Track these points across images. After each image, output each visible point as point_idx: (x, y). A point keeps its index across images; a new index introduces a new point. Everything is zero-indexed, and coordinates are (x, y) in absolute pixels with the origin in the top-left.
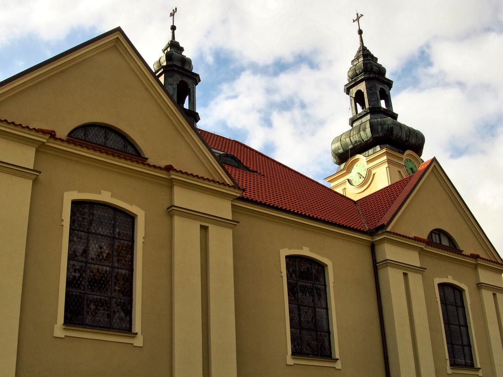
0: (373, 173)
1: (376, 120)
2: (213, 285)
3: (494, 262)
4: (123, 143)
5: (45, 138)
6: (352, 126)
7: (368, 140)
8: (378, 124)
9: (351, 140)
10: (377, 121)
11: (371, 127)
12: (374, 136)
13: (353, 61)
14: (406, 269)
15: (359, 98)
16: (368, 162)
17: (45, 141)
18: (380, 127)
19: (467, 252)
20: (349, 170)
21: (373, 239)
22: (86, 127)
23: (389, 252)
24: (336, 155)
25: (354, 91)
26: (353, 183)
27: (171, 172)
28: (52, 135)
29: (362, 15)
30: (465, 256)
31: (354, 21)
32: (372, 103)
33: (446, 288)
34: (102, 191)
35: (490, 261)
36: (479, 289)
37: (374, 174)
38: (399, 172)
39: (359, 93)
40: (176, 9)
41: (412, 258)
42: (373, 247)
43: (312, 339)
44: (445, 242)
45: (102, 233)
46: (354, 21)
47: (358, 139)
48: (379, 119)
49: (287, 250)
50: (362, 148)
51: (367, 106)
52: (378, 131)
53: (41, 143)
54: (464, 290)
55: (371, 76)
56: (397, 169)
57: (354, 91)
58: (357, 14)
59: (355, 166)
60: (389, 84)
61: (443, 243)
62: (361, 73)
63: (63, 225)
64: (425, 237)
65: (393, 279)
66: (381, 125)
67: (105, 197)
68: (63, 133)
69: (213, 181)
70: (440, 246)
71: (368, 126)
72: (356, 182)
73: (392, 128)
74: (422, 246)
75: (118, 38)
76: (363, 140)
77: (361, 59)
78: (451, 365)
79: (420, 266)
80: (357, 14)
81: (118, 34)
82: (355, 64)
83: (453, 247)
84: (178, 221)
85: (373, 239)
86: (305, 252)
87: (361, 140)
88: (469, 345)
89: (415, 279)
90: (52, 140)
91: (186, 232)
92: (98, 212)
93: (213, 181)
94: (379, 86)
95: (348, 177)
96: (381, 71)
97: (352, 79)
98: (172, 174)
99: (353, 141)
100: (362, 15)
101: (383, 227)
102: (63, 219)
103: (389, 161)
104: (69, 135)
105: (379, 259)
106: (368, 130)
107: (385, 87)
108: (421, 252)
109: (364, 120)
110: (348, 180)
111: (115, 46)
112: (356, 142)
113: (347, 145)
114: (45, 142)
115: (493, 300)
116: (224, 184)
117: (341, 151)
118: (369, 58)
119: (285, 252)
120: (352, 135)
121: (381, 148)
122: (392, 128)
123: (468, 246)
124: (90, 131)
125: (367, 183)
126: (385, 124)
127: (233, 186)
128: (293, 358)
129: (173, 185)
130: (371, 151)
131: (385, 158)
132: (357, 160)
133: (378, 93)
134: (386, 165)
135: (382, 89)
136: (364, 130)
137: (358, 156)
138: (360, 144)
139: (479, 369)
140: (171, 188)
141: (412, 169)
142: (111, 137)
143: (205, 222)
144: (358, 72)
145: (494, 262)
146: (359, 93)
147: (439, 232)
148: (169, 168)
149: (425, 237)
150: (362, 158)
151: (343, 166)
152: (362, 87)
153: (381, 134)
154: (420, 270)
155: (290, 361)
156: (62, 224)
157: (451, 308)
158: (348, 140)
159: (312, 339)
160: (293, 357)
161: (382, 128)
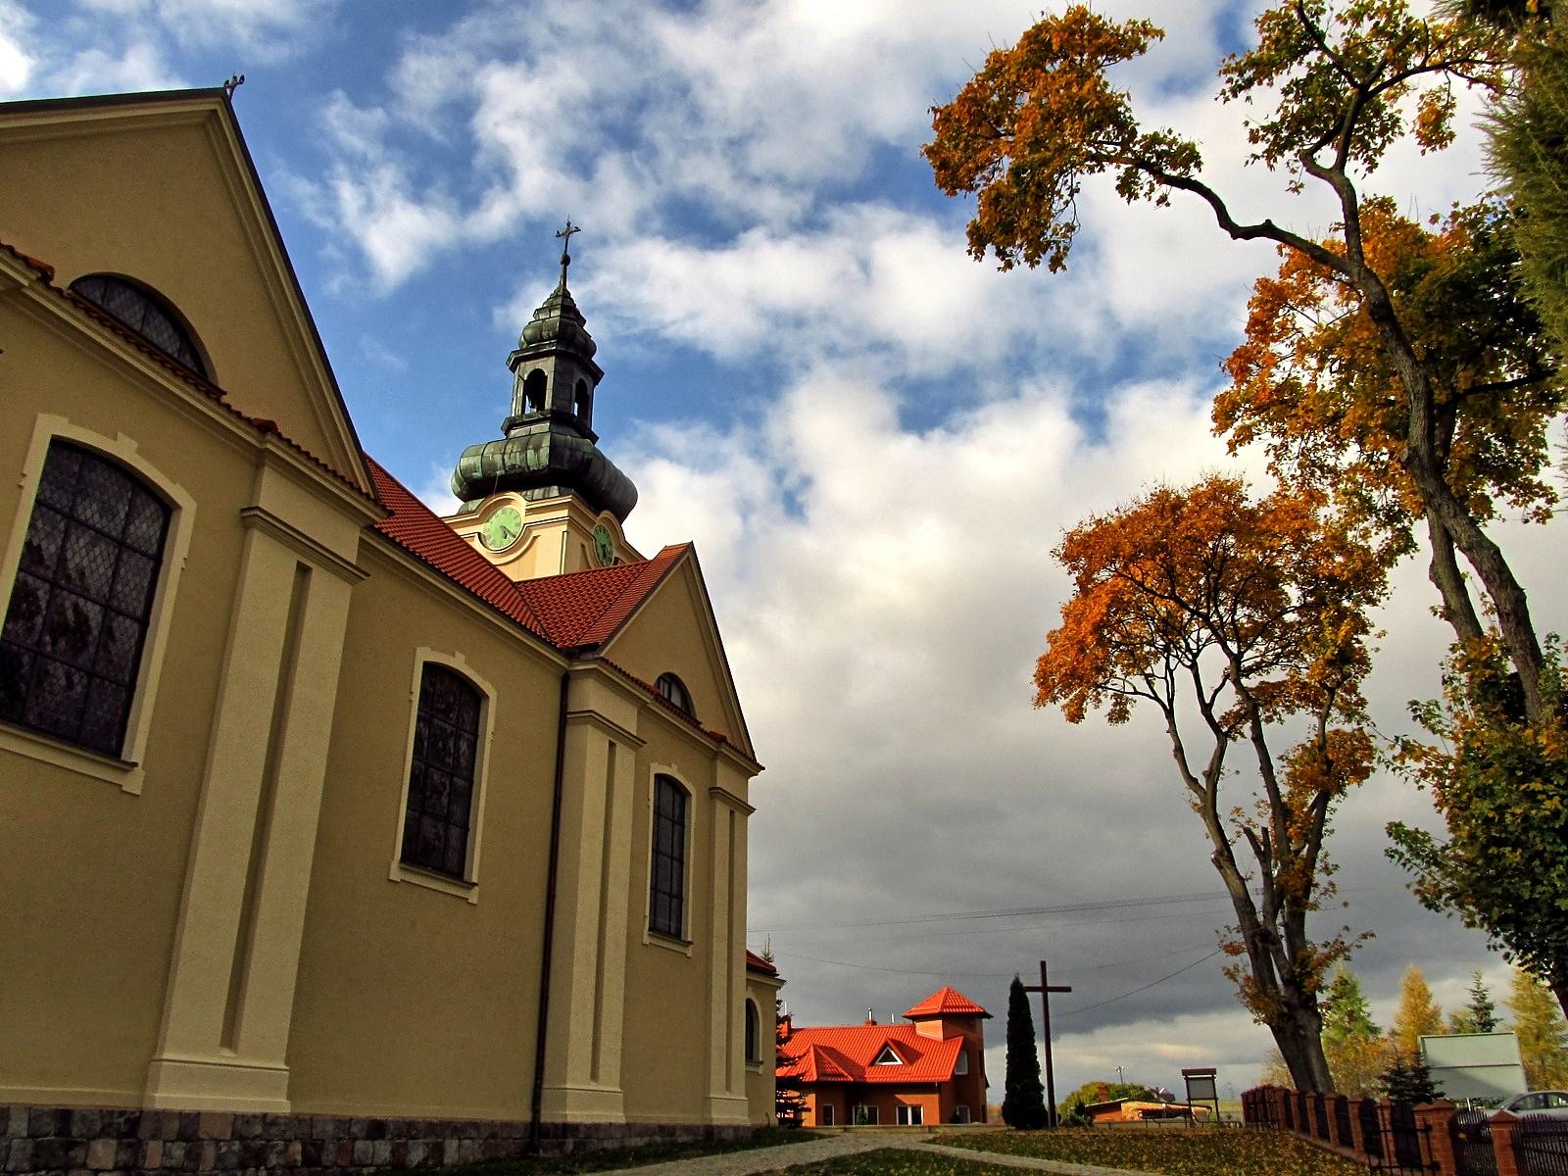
0: (534, 533)
1: (562, 437)
2: (299, 690)
3: (739, 752)
4: (178, 345)
5: (27, 278)
6: (506, 434)
7: (539, 470)
8: (565, 446)
9: (503, 460)
10: (566, 441)
11: (553, 447)
12: (552, 466)
13: (538, 311)
14: (616, 734)
15: (534, 386)
16: (529, 511)
17: (25, 283)
18: (568, 453)
19: (707, 727)
20: (485, 515)
21: (570, 666)
22: (111, 282)
23: (592, 696)
24: (466, 479)
25: (528, 367)
26: (488, 542)
27: (269, 437)
28: (45, 274)
29: (577, 230)
30: (702, 731)
31: (558, 235)
32: (559, 403)
33: (663, 784)
34: (120, 434)
35: (732, 747)
36: (711, 798)
37: (535, 538)
38: (583, 546)
39: (537, 377)
40: (242, 78)
41: (626, 717)
42: (566, 681)
43: (436, 841)
44: (676, 700)
45: (98, 526)
46: (558, 235)
47: (518, 463)
48: (569, 437)
49: (427, 649)
50: (521, 480)
51: (548, 405)
52: (562, 458)
53: (13, 285)
54: (690, 795)
55: (570, 351)
56: (578, 540)
57: (528, 367)
58: (569, 224)
59: (499, 512)
60: (596, 375)
61: (673, 700)
62: (549, 339)
63: (21, 487)
64: (651, 682)
65: (591, 746)
66: (571, 449)
67: (124, 449)
68: (62, 280)
69: (334, 473)
70: (666, 702)
71: (546, 443)
72: (493, 543)
73: (590, 461)
74: (647, 698)
75: (214, 111)
76: (529, 467)
77: (556, 313)
78: (650, 929)
79: (635, 734)
80: (569, 224)
81: (219, 103)
82: (542, 317)
83: (686, 711)
84: (259, 545)
85: (570, 666)
86: (457, 662)
87: (524, 465)
88: (680, 898)
89: (625, 757)
90: (40, 287)
91: (268, 568)
92: (98, 475)
93: (334, 473)
94: (579, 376)
95: (480, 528)
96: (588, 348)
97: (529, 343)
98: (268, 442)
99: (508, 463)
100: (577, 230)
101: (594, 647)
102: (25, 472)
103: (571, 522)
104: (72, 286)
105: (574, 706)
106: (545, 452)
107: (589, 382)
108: (643, 708)
109: (535, 429)
110: (479, 534)
111: (203, 126)
112: (513, 466)
113: (493, 466)
114: (23, 286)
115: (728, 822)
116: (354, 487)
117: (478, 474)
118: (572, 316)
119: (426, 654)
120: (508, 451)
121: (561, 495)
122: (590, 461)
123: (709, 718)
124: (116, 293)
125: (515, 551)
126: (578, 449)
127: (367, 495)
128: (402, 868)
129: (263, 465)
130: (538, 493)
131: (565, 513)
132: (509, 501)
133: (574, 386)
134: (565, 528)
135: (581, 380)
136: (537, 449)
137: (512, 495)
138: (520, 474)
139: (691, 943)
140: (258, 467)
141: (604, 546)
142: (157, 322)
143: (310, 557)
144: (545, 334)
145: (739, 752)
146: (537, 377)
147: (670, 679)
148: (266, 428)
149: (651, 682)
150: (518, 502)
151: (474, 505)
152: (547, 366)
153: (566, 467)
154: (635, 743)
155: (396, 874)
156: (22, 484)
157: (666, 824)
158: (498, 458)
159: (436, 841)
160: (403, 865)
161: (571, 456)
